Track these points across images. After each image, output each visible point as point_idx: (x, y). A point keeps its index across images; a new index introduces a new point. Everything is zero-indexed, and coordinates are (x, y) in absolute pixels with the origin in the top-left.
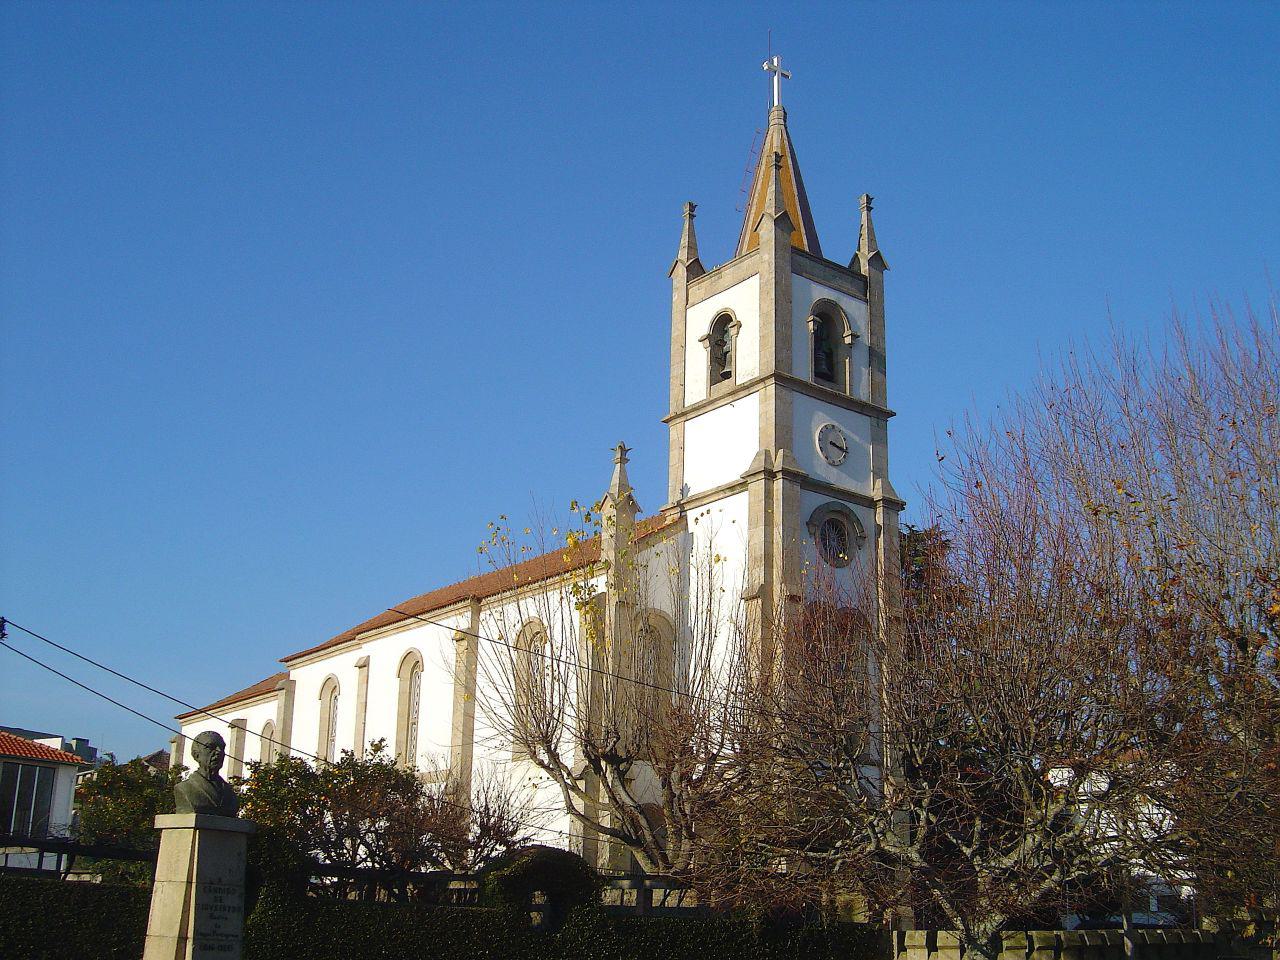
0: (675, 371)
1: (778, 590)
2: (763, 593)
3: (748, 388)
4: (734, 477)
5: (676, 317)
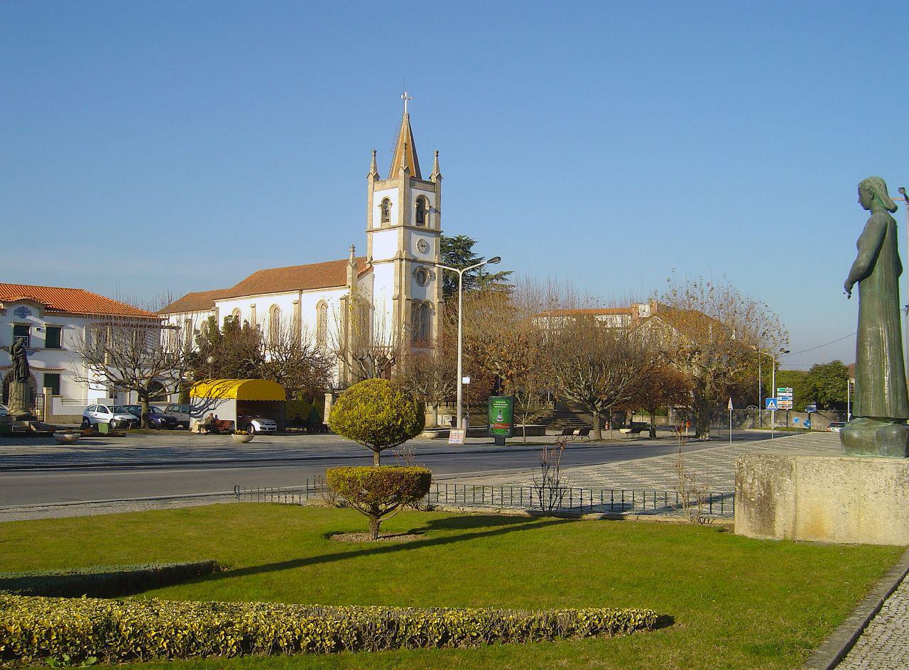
0: (369, 214)
1: (404, 297)
2: (398, 298)
3: (394, 227)
4: (389, 258)
5: (370, 194)
